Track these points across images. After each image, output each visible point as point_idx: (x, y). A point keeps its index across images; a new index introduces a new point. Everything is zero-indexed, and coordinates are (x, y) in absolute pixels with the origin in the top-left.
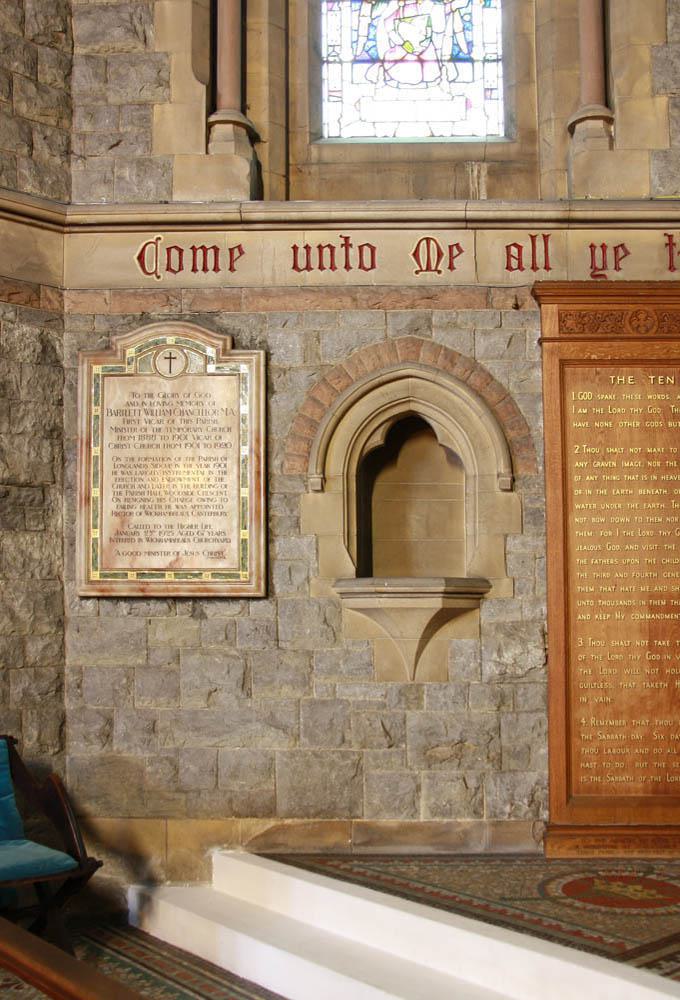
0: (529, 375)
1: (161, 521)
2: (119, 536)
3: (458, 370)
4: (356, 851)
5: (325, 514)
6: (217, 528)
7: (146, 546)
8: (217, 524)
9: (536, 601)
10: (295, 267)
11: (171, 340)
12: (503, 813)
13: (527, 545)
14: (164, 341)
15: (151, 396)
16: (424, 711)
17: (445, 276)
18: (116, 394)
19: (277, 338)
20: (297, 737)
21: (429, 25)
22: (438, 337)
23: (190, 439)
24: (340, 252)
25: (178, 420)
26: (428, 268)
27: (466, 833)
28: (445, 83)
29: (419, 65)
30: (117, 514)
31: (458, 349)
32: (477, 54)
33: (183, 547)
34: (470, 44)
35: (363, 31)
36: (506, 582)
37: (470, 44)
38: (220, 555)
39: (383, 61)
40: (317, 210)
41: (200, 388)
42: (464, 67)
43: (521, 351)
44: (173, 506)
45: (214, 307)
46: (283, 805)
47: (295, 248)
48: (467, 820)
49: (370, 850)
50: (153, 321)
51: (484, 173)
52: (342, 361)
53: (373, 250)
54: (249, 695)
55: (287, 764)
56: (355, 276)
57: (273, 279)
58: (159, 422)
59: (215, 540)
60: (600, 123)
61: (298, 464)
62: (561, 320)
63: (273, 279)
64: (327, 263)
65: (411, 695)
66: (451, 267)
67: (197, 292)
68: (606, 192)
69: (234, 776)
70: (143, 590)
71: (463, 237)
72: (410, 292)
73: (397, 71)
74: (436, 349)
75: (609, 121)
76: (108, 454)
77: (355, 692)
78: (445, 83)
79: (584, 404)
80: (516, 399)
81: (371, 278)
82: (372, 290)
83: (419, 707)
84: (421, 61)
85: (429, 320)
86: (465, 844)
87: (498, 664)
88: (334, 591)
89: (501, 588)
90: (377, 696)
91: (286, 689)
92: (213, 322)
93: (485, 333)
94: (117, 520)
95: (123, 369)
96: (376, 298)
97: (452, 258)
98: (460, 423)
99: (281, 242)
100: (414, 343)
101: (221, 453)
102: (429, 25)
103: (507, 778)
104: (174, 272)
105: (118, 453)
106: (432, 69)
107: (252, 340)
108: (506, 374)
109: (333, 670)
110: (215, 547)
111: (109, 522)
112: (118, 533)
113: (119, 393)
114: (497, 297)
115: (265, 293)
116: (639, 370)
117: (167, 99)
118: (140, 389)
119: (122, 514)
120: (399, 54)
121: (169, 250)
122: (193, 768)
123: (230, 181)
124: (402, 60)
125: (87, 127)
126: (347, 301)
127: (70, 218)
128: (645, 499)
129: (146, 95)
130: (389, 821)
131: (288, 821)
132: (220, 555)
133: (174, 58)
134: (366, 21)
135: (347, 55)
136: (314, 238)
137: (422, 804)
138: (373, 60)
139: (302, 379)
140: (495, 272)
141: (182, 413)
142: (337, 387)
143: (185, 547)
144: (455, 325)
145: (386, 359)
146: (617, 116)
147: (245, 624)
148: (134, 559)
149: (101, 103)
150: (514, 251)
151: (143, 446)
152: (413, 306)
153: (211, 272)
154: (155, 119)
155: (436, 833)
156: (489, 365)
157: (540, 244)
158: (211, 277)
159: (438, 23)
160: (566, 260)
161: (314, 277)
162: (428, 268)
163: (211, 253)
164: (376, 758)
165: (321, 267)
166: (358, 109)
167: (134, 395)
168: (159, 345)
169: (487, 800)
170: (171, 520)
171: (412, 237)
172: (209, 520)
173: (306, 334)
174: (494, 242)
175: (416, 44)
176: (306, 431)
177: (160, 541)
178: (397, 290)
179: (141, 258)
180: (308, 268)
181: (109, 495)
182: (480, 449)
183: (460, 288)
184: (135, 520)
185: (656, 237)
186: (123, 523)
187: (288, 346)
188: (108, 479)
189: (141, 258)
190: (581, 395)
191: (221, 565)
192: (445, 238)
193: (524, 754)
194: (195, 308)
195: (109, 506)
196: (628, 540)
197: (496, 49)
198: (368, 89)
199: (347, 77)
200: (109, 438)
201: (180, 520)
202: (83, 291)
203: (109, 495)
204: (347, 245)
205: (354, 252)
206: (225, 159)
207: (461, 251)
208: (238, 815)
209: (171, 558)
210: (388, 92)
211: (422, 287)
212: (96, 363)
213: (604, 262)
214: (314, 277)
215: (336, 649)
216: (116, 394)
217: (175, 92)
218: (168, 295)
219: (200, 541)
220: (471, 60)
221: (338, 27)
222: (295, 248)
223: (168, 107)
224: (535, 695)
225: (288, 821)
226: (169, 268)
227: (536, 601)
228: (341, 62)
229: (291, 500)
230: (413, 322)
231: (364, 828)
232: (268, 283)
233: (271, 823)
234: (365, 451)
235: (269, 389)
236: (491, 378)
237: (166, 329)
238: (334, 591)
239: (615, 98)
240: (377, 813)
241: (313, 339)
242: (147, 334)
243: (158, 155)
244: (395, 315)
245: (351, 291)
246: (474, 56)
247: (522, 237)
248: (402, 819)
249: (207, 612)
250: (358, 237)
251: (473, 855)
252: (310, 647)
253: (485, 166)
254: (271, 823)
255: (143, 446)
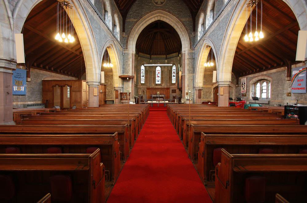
5: (142, 93)
43: (146, 89)
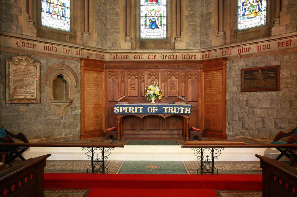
0: (78, 71)
1: (23, 90)
2: (14, 92)
3: (69, 69)
4: (53, 142)
5: (49, 90)
6: (32, 92)
7: (20, 94)
9: (79, 103)
10: (44, 49)
11: (24, 59)
12: (74, 134)
13: (78, 95)
14: (23, 59)
15: (20, 68)
16: (63, 120)
17: (67, 54)
18: (14, 67)
19: (42, 61)
20: (44, 125)
21: (59, 9)
22: (66, 64)
23: (28, 76)
24: (52, 48)
25: (25, 73)
26: (65, 53)
27: (69, 138)
28: (61, 20)
29: (57, 16)
30: (14, 89)
31: (69, 66)
32: (66, 16)
33: (26, 95)
34: (65, 14)
35: (48, 7)
36: (75, 101)
37: (65, 14)
38: (33, 96)
39: (51, 14)
40: (49, 41)
41: (29, 68)
42: (64, 18)
43: (77, 67)
44: (25, 88)
45: (31, 54)
46: (42, 136)
47: (44, 46)
48: (69, 136)
49: (55, 142)
50: (19, 55)
51: (68, 37)
52: (52, 66)
53: (57, 49)
54: (36, 119)
55: (43, 130)
56: (54, 52)
57: (41, 51)
58: (22, 73)
59: (32, 94)
60: (88, 35)
61: (45, 82)
62: (84, 64)
63: (41, 51)
64: (50, 50)
65: (62, 118)
66: (68, 53)
67: (28, 51)
68: (89, 45)
69: (34, 132)
70: (19, 102)
71: (70, 49)
72: (63, 56)
73: (53, 16)
74: (66, 65)
75: (89, 35)
76: (12, 78)
77: (53, 118)
78: (61, 20)
79: (86, 76)
80: (77, 74)
81: (56, 53)
82: (57, 55)
83: (63, 119)
84: (58, 15)
85: (65, 61)
86: (69, 140)
87: (75, 113)
88: (50, 102)
89: (75, 102)
90: (57, 118)
91: (43, 117)
92: (30, 57)
93: (73, 64)
94: (14, 90)
95: (15, 63)
96: (58, 57)
97: (68, 52)
98: (69, 78)
99: (42, 45)
100: (63, 64)
101: (33, 79)
102: (59, 9)
103: (75, 129)
104: (23, 47)
105: (14, 78)
106: (59, 17)
107: (37, 61)
108: (76, 70)
109: (50, 114)
110: (32, 95)
112: (14, 92)
113: (14, 67)
114: (75, 58)
115: (40, 53)
116: (93, 72)
117: (21, 15)
118: (18, 67)
119: (15, 89)
120: (54, 13)
121: (22, 43)
122: (27, 132)
123: (33, 33)
124: (54, 14)
125: (5, 17)
126: (53, 56)
127: (4, 34)
128: (93, 89)
129: (18, 14)
130: (58, 137)
131: (43, 139)
132: (33, 96)
133: (23, 8)
134: (48, 6)
135: (45, 11)
136: (48, 45)
137: (63, 134)
138: (50, 13)
139: (46, 68)
140: (74, 55)
141: (26, 72)
142: (51, 70)
143: (27, 95)
144: (68, 62)
145: (59, 66)
146: (91, 34)
147: (36, 107)
148: (17, 97)
149: (8, 12)
150: (170, 56)
151: (19, 77)
152: (63, 58)
153: (30, 48)
154: (19, 18)
155: (65, 138)
156: (73, 69)
157: (80, 52)
158: (30, 49)
159: (60, 10)
160: (84, 54)
161: (47, 52)
162: (65, 53)
163: (30, 45)
164: (57, 127)
165: (49, 50)
166: (47, 21)
167: (17, 68)
168: (22, 59)
169: (72, 133)
170: (25, 90)
171: (63, 47)
172: (31, 90)
173: (47, 61)
174: (74, 50)
175: (57, 12)
176: (46, 76)
177: (22, 93)
178: (61, 56)
179: (17, 43)
180: (47, 50)
182: (72, 81)
183: (70, 57)
184: (17, 90)
185: (95, 53)
186: (15, 90)
187: (43, 62)
188: (12, 82)
189: (17, 43)
190: (86, 74)
191: (33, 98)
192: (68, 48)
193: (77, 126)
194: (27, 54)
195: (13, 87)
196: (91, 95)
197: (69, 16)
198: (49, 18)
199: (45, 15)
200: (12, 75)
201: (26, 90)
202: (6, 47)
204: (53, 47)
205: (54, 48)
206: (32, 29)
207: (70, 51)
208: (34, 139)
209: (24, 96)
210: (52, 19)
211: (64, 56)
212: (10, 62)
213: (261, 48)
214: (47, 52)
215: (51, 111)
216: (14, 67)
217: (23, 14)
218: (23, 51)
219: (29, 94)
220: (65, 17)
221: (44, 5)
222: (44, 46)
223: (21, 17)
224: (79, 117)
225: (43, 139)
226: (22, 46)
227: (79, 103)
228: (44, 12)
229: (44, 87)
230: (63, 61)
231: (54, 139)
232: (40, 51)
233: (40, 139)
234: (64, 77)
235: (41, 70)
236: (73, 71)
237: (23, 57)
238: (50, 102)
239: (90, 31)
240: (57, 136)
241: (47, 62)
242: (20, 57)
243: (19, 25)
244: (60, 59)
245: (54, 55)
246: (66, 16)
247: (78, 50)
248: (60, 137)
249: (30, 106)
250: (54, 46)
251: (70, 141)
252: (46, 111)
253: (68, 36)
254: (40, 139)
255: (19, 77)
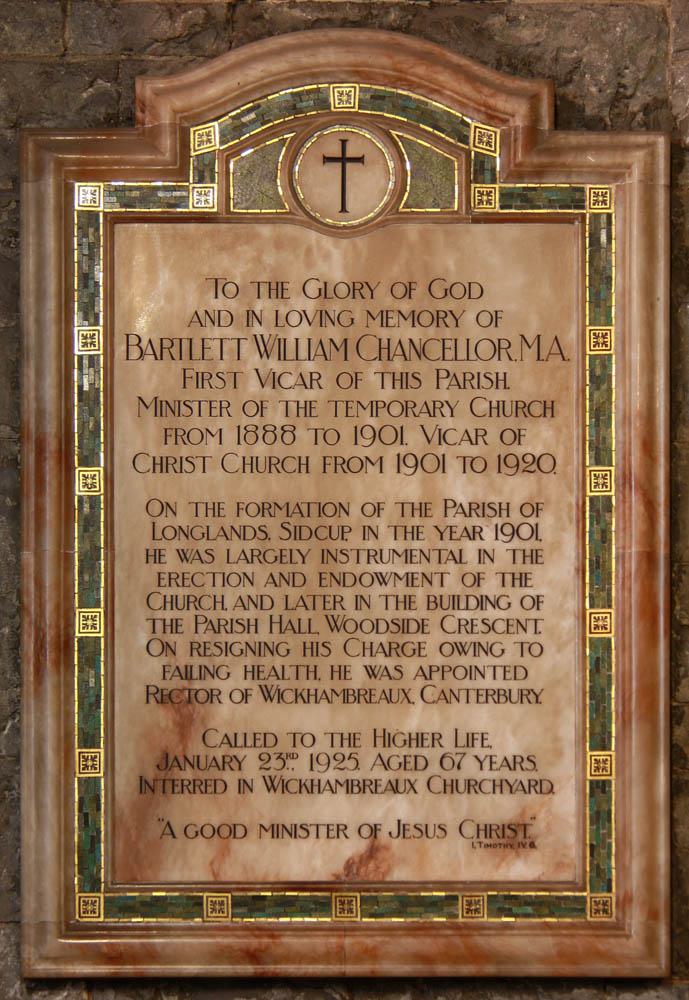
2: (165, 776)
8: (507, 731)
38: (514, 837)
111: (134, 727)
132: (514, 837)
181: (136, 635)
195: (137, 668)
200: (135, 435)
203: (136, 635)
